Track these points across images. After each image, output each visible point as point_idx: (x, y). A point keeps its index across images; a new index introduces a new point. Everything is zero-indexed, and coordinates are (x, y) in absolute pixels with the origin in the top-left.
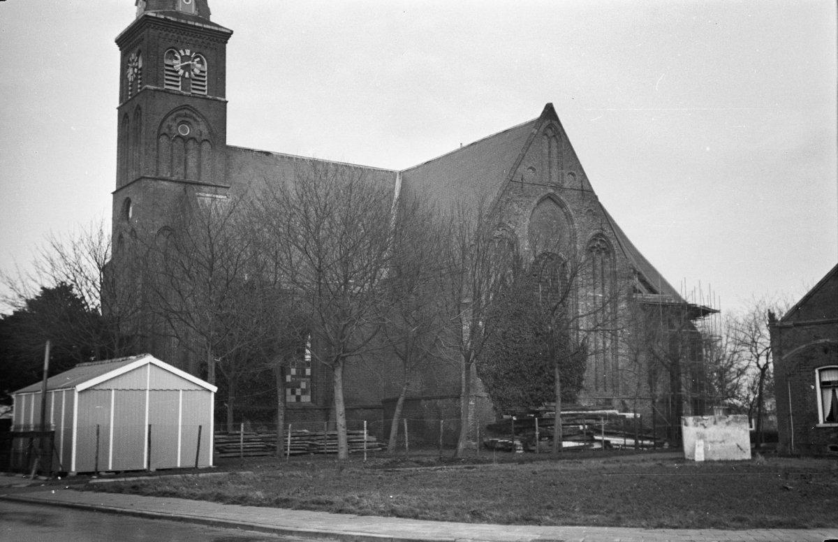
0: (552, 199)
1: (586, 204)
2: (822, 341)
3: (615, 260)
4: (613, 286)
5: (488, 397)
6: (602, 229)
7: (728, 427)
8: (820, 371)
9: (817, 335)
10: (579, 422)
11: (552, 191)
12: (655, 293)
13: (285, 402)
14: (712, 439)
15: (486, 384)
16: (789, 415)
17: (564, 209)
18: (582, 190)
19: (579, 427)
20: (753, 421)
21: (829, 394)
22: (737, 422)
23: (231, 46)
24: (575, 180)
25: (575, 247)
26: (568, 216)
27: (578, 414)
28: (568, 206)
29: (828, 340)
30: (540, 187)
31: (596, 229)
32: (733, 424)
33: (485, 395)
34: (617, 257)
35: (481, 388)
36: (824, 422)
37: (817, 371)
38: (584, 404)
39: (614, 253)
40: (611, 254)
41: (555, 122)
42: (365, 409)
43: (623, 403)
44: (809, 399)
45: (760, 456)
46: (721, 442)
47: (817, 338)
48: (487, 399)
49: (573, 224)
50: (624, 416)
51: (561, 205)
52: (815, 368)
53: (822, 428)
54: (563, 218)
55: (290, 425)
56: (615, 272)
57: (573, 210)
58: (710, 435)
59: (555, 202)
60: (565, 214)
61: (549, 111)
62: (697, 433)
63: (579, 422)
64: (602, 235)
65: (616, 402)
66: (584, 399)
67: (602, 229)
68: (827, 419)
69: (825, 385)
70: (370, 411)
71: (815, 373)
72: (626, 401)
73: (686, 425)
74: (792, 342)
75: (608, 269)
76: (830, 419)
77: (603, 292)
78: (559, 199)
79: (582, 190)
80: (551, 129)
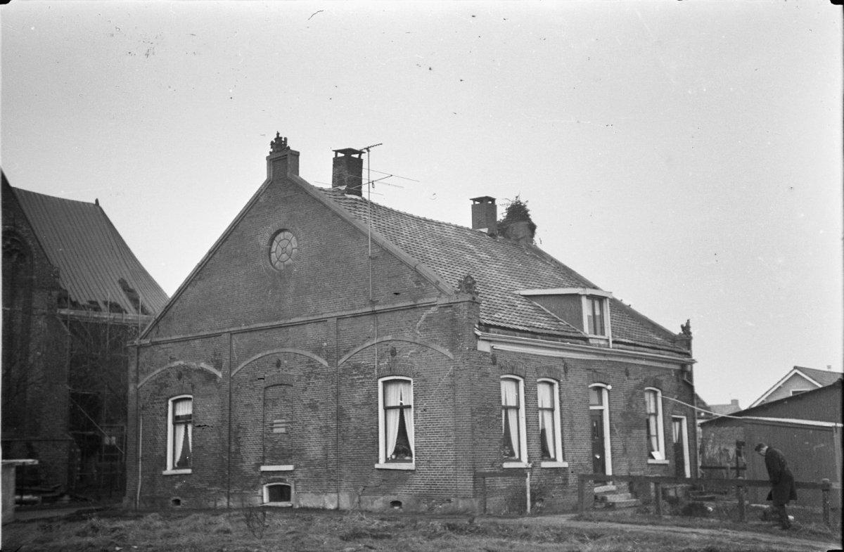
2: (176, 363)
6: (14, 225)
8: (175, 402)
9: (173, 357)
12: (146, 314)
13: (704, 457)
16: (137, 461)
21: (181, 430)
23: (301, 158)
29: (182, 363)
36: (174, 468)
37: (170, 403)
39: (32, 257)
44: (160, 438)
45: (477, 502)
47: (172, 359)
52: (168, 399)
53: (172, 476)
67: (14, 225)
68: (178, 464)
69: (177, 420)
71: (167, 405)
72: (34, 444)
74: (148, 366)
76: (183, 464)
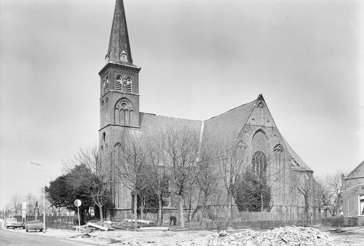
11: (261, 128)
26: (267, 137)
28: (267, 134)
41: (263, 101)
51: (264, 133)
57: (269, 135)
59: (262, 132)
61: (261, 97)
64: (280, 144)
67: (280, 142)
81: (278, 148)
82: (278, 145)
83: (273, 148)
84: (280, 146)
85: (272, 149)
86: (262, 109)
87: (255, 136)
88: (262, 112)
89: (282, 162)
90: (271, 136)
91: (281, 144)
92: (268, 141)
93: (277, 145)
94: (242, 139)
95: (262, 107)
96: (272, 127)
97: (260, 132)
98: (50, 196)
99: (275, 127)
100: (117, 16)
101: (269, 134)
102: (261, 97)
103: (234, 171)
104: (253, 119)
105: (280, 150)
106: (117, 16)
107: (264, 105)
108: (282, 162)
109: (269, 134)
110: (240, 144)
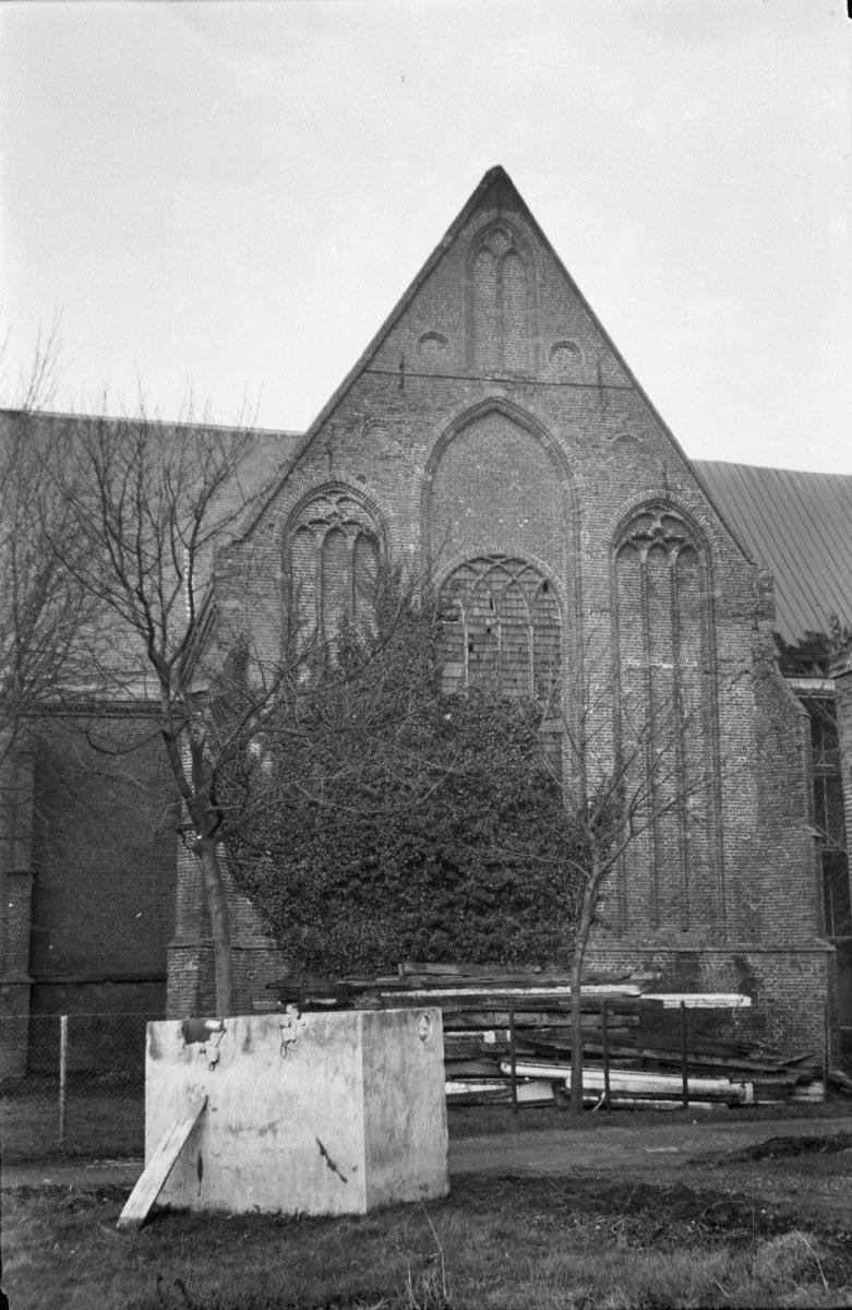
0: (506, 416)
1: (612, 423)
3: (711, 570)
4: (710, 639)
5: (270, 950)
7: (288, 1065)
10: (481, 1020)
11: (499, 392)
14: (249, 1125)
15: (264, 913)
17: (543, 439)
18: (601, 387)
19: (482, 1037)
20: (625, 1030)
22: (322, 1042)
24: (579, 361)
25: (577, 538)
26: (555, 454)
27: (484, 998)
28: (555, 430)
30: (459, 383)
31: (646, 488)
32: (307, 1050)
33: (261, 942)
34: (718, 561)
35: (250, 926)
38: (595, 966)
39: (709, 550)
40: (702, 554)
41: (514, 217)
42: (118, 982)
43: (741, 964)
46: (262, 1132)
48: (267, 955)
49: (570, 476)
50: (661, 1002)
51: (535, 430)
54: (544, 464)
55: (64, 1019)
56: (713, 600)
57: (570, 439)
58: (227, 1103)
59: (516, 422)
60: (550, 453)
61: (497, 190)
62: (189, 1090)
63: (481, 1020)
64: (668, 503)
65: (714, 964)
66: (603, 954)
67: (666, 486)
70: (134, 988)
73: (156, 1055)
75: (692, 593)
77: (675, 655)
78: (530, 416)
79: (601, 387)
80: (504, 233)
81: (658, 532)
82: (654, 504)
83: (607, 533)
84: (673, 513)
85: (595, 534)
86: (513, 269)
87: (456, 450)
88: (516, 290)
89: (692, 628)
90: (587, 444)
91: (673, 498)
92: (566, 485)
93: (646, 504)
94: (342, 475)
95: (512, 252)
96: (593, 381)
97: (494, 422)
98: (730, 865)
99: (621, 379)
100: (793, 670)
101: (576, 429)
102: (497, 190)
103: (669, 789)
104: (432, 336)
105: (673, 540)
106: (793, 670)
107: (526, 244)
108: (692, 628)
109: (576, 429)
110: (322, 510)
